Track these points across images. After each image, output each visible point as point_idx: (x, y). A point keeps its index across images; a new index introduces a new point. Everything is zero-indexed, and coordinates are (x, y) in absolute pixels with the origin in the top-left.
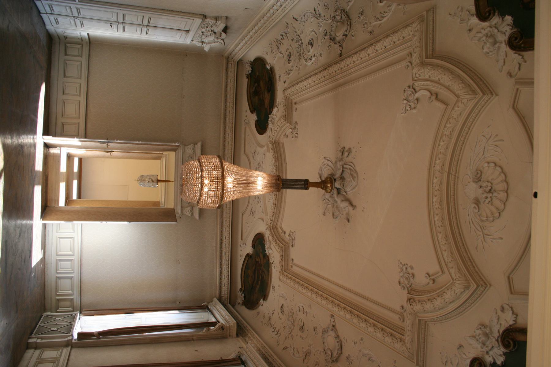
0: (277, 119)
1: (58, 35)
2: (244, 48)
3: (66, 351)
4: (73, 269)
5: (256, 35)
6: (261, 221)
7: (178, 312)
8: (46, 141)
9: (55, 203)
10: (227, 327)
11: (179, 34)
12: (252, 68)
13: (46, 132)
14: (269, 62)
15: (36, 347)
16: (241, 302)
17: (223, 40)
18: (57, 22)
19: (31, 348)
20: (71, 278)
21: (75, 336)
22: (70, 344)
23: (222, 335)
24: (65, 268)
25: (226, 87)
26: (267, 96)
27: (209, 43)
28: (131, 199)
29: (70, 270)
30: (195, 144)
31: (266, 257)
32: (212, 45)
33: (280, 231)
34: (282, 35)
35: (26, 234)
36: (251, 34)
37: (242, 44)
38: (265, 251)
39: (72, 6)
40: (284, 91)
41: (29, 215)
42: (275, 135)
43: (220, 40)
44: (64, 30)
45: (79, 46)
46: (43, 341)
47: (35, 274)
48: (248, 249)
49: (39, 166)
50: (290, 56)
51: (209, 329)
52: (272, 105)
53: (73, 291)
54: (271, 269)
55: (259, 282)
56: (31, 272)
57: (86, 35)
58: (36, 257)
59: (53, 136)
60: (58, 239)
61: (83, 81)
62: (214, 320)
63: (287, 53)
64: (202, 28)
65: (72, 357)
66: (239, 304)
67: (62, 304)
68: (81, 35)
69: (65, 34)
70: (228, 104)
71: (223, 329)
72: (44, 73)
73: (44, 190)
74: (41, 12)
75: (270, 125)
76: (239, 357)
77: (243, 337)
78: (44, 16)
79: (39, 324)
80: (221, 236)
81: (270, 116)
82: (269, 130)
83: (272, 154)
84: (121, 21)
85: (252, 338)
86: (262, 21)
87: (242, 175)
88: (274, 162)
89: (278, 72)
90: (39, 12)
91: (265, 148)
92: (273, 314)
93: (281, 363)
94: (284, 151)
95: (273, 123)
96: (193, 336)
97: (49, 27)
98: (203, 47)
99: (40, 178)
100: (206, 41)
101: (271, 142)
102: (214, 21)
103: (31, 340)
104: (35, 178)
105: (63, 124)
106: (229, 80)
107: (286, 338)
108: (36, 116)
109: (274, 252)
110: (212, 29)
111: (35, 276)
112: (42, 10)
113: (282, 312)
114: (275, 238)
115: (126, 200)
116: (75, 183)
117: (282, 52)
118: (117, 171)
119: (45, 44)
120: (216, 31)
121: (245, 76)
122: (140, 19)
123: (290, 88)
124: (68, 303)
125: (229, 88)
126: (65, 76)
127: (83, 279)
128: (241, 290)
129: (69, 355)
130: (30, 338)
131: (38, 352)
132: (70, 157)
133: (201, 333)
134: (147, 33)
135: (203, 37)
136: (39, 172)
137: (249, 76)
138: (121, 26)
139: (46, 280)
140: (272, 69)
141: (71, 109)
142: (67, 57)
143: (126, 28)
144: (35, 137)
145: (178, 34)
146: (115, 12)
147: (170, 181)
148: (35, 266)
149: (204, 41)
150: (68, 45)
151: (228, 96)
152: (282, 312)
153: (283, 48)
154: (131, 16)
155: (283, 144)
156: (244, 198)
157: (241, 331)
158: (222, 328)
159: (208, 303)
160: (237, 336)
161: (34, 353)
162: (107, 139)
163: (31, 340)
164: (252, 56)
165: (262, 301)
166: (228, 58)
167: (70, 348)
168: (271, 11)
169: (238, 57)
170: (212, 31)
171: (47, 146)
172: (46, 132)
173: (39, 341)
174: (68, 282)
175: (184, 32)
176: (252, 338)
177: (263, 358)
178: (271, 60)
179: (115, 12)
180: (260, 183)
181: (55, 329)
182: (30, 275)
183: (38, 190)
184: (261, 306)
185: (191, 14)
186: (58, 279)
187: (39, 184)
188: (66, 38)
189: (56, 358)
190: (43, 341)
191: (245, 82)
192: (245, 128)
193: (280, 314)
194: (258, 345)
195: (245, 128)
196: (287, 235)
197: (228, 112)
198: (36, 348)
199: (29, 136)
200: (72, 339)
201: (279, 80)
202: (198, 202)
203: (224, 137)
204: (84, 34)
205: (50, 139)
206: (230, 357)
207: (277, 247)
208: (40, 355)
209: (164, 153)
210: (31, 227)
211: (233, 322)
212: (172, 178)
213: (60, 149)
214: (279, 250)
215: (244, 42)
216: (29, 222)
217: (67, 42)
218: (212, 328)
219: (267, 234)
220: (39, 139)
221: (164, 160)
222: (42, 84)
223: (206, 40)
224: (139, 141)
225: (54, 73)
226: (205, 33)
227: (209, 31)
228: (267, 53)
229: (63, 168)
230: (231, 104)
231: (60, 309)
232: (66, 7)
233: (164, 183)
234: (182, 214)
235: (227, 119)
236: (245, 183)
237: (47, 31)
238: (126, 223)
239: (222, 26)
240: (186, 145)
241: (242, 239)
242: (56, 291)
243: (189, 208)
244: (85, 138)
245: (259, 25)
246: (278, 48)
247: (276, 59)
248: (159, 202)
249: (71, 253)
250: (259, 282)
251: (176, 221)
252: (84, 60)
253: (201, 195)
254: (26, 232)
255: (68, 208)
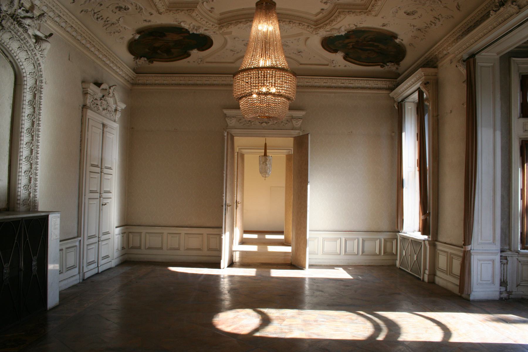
0: (194, 23)
1: (122, 256)
2: (118, 65)
3: (440, 247)
4: (353, 239)
5: (101, 50)
6: (308, 42)
7: (403, 134)
8: (226, 265)
9: (288, 256)
10: (425, 79)
11: (108, 135)
12: (141, 57)
13: (217, 265)
14: (131, 37)
15: (433, 274)
16: (396, 66)
17: (110, 88)
18: (107, 257)
19: (434, 280)
20: (363, 241)
21: (426, 237)
22: (433, 243)
23: (434, 85)
24: (354, 246)
25: (164, 85)
26: (171, 37)
27: (116, 103)
28: (283, 183)
29: (356, 241)
30: (225, 116)
31: (351, 34)
32: (117, 100)
33: (321, 15)
34: (97, 18)
35: (320, 285)
36: (101, 56)
37: (115, 68)
38: (342, 35)
39: (86, 243)
40: (160, 13)
41: (301, 281)
42: (212, 24)
43: (111, 91)
44: (115, 251)
45: (131, 236)
46: (428, 268)
47: (359, 275)
48: (339, 57)
49: (251, 272)
50: (120, 8)
51: (427, 99)
52: (178, 30)
53: (377, 239)
54: (363, 28)
55: (376, 44)
56: (358, 279)
57: (118, 229)
58: (342, 274)
59: (221, 259)
60: (324, 253)
61: (166, 231)
62: (416, 95)
63: (118, 12)
64: (98, 109)
65: (448, 241)
66: (397, 69)
67: (388, 250)
68: (119, 234)
69: (120, 249)
70: (182, 82)
71: (428, 83)
72: (158, 268)
73: (275, 266)
74: (97, 272)
75: (201, 31)
76: (464, 61)
77: (437, 61)
78: (101, 270)
79: (409, 271)
80: (324, 87)
81: (191, 32)
82: (207, 33)
83: (232, 26)
84: (99, 194)
85: (441, 49)
86: (84, 42)
87: (256, 49)
88: (242, 25)
89: (143, 25)
90: (98, 274)
91: (227, 36)
92: (414, 26)
93: (476, 11)
94: (229, 12)
95: (199, 27)
96: (433, 116)
97: (113, 264)
98: (122, 109)
99: (263, 271)
100: (114, 106)
101: (220, 28)
102: (89, 96)
103: (426, 279)
104: (263, 276)
105: (209, 249)
106: (157, 82)
107: (445, 7)
108: (201, 275)
109: (345, 24)
110: (99, 99)
111: (361, 276)
112: (95, 271)
113: (413, 13)
114: (328, 22)
115: (284, 189)
116: (268, 237)
117: (117, 18)
118: (255, 197)
119: (130, 268)
120: (100, 95)
121: (151, 65)
122: (93, 175)
123: (155, 5)
124: (389, 244)
125: (165, 82)
126: (161, 248)
127: (365, 230)
128: (382, 66)
129: (445, 243)
130: (423, 280)
131: (438, 273)
132: (243, 242)
133: (430, 108)
134: (110, 168)
135: (109, 109)
136: (257, 272)
137: (151, 60)
138: (104, 195)
139: (365, 264)
140: (139, 32)
141: (194, 242)
142: (143, 247)
143: (105, 189)
144: (222, 276)
145: (107, 135)
146: (89, 201)
147: (266, 144)
148: (351, 275)
149: (114, 108)
150: (131, 246)
151: (173, 82)
152: (413, 13)
153: (113, 18)
154: (92, 184)
155: (221, 14)
156: (284, 45)
157: (430, 63)
158: (426, 84)
159: (395, 102)
160: (436, 67)
161: (439, 277)
162: (223, 206)
163: (426, 279)
164: (129, 57)
165: (397, 41)
166: (133, 84)
167: (437, 243)
168: (69, 29)
169: (131, 73)
170: (101, 99)
171: (231, 264)
172: (217, 265)
173: (427, 272)
174: (367, 244)
175: (105, 130)
176: (441, 49)
177: (467, 34)
178: (129, 35)
179: (89, 201)
180: (265, 27)
181: (415, 256)
182: (362, 280)
183: (275, 273)
184: (403, 42)
185: (83, 121)
186: (364, 254)
187: (269, 272)
188: (123, 248)
189: (447, 256)
190: (428, 268)
191: (157, 65)
192: (207, 62)
193: (416, 16)
194: (450, 42)
195: (207, 62)
196: (325, 7)
197: (190, 82)
198: (434, 275)
199: (222, 283)
200: (428, 240)
201: (150, 21)
202: (288, 98)
203: (218, 85)
204: (117, 231)
205: (225, 261)
206: (464, 72)
207: (339, 19)
208: (442, 271)
209: (237, 150)
210: (312, 280)
211: (420, 72)
212: (260, 141)
213: (234, 251)
214: (342, 16)
215: (111, 65)
216: (307, 282)
217: (127, 247)
218: (425, 96)
219: (323, 33)
220: (224, 272)
221: (244, 151)
222: (170, 270)
223: (114, 107)
224: (223, 173)
225: (159, 259)
226: (105, 107)
227: (102, 103)
228: (122, 38)
229: (253, 248)
230: (182, 79)
231: (394, 252)
232: (88, 250)
233: (268, 151)
234: (300, 129)
235: (198, 82)
236: (266, 44)
237: (117, 266)
238: (309, 186)
239: (92, 88)
240: (227, 126)
241: (327, 65)
242: (376, 255)
243: (294, 122)
244: (222, 228)
245: (88, 45)
246: (113, 24)
247: (127, 27)
248: (287, 155)
249: (339, 241)
250: (376, 44)
251: (308, 134)
252: (143, 230)
253: (280, 95)
254: (318, 284)
255: (293, 243)
